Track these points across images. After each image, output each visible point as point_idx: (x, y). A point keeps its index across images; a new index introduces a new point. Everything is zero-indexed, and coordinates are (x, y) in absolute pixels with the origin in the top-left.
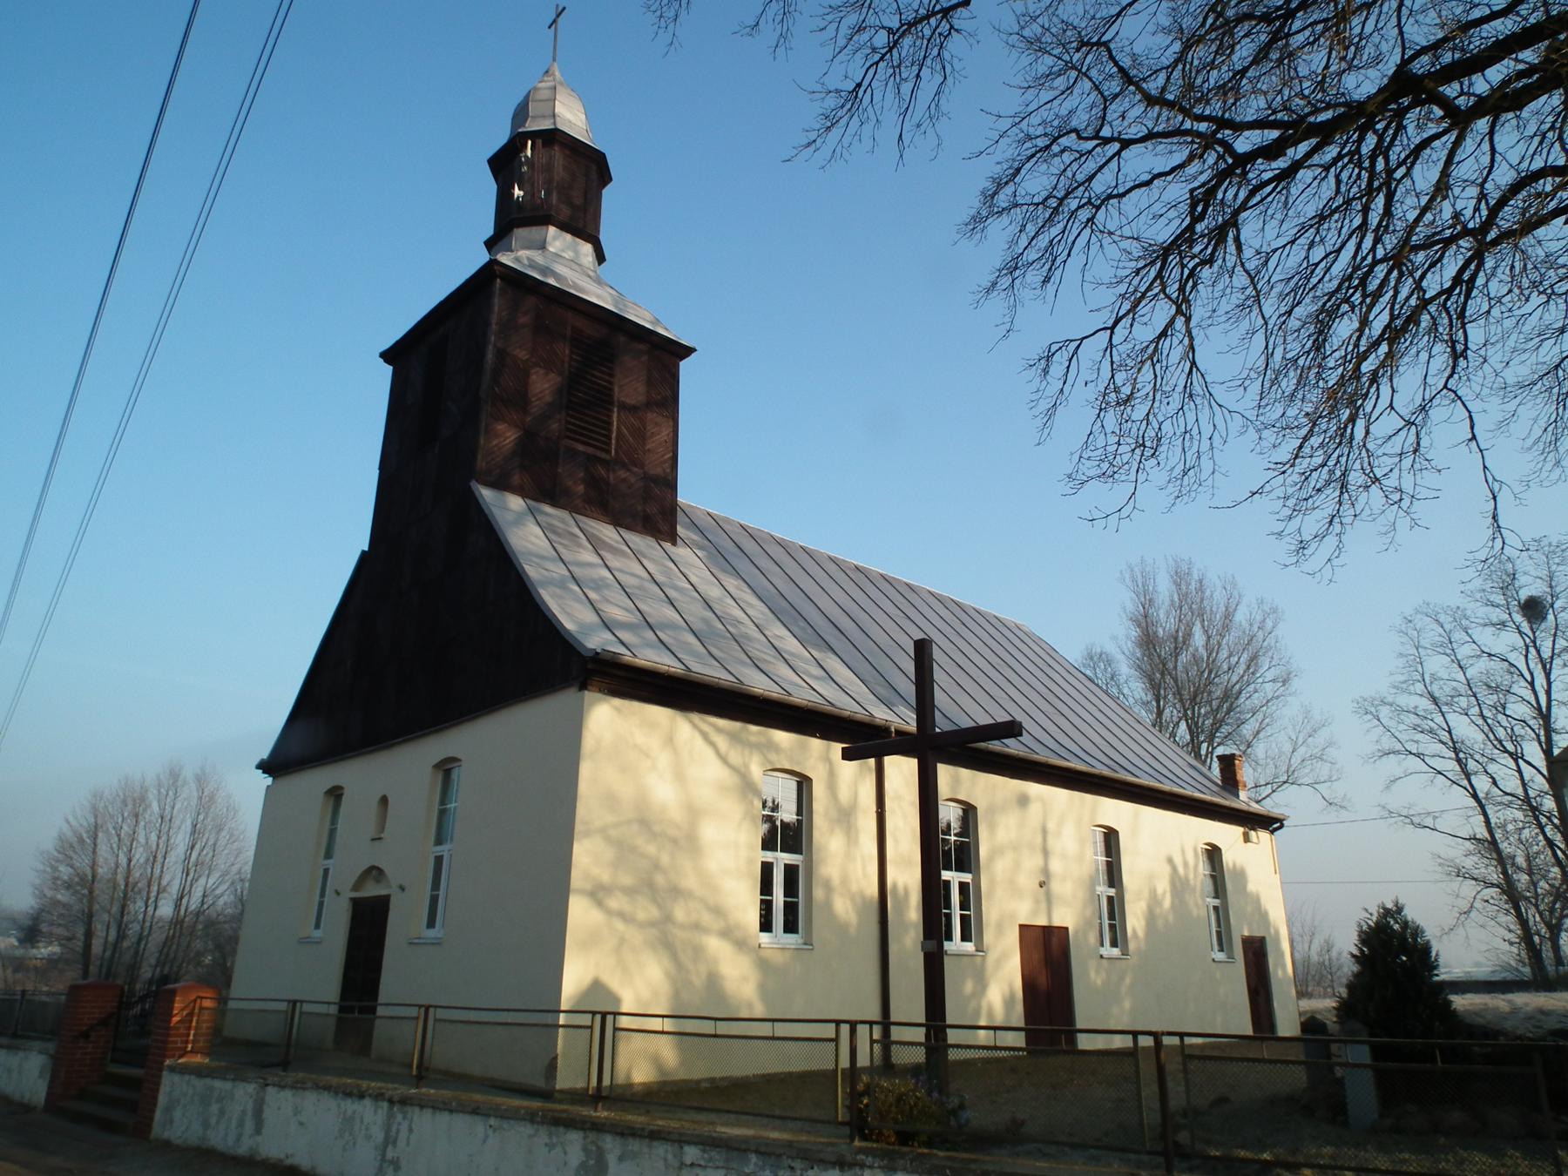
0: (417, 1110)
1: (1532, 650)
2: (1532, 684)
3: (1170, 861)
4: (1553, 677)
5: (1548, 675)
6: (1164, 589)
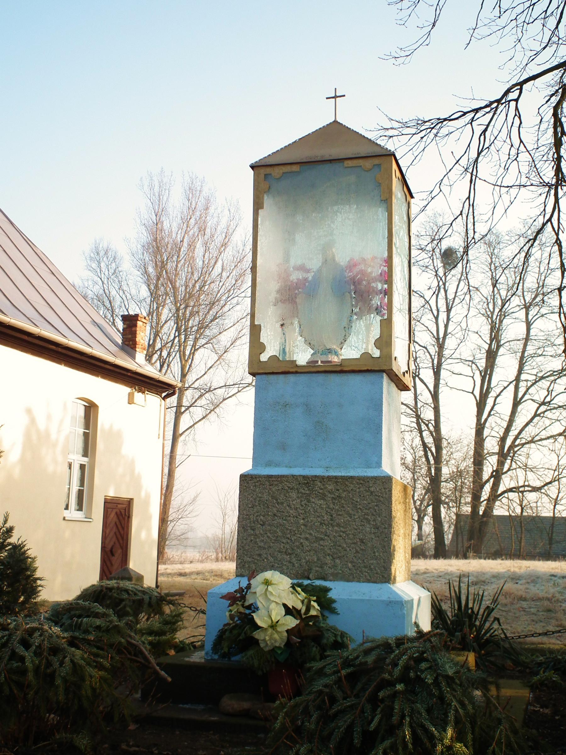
1: (442, 291)
2: (437, 318)
3: (29, 411)
4: (452, 314)
5: (449, 310)
6: (176, 204)
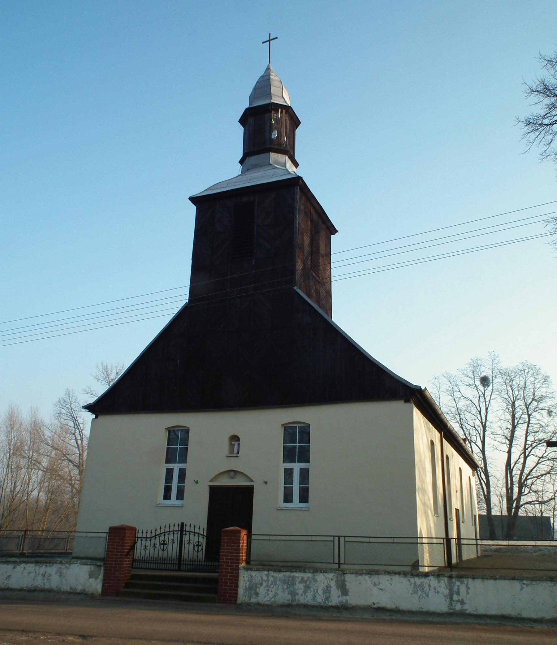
0: (470, 580)
2: (480, 412)
